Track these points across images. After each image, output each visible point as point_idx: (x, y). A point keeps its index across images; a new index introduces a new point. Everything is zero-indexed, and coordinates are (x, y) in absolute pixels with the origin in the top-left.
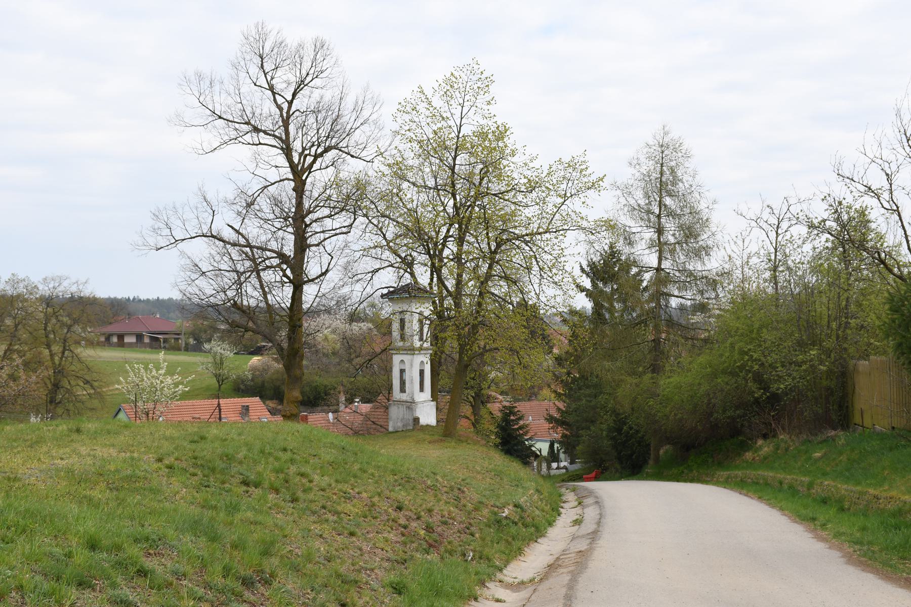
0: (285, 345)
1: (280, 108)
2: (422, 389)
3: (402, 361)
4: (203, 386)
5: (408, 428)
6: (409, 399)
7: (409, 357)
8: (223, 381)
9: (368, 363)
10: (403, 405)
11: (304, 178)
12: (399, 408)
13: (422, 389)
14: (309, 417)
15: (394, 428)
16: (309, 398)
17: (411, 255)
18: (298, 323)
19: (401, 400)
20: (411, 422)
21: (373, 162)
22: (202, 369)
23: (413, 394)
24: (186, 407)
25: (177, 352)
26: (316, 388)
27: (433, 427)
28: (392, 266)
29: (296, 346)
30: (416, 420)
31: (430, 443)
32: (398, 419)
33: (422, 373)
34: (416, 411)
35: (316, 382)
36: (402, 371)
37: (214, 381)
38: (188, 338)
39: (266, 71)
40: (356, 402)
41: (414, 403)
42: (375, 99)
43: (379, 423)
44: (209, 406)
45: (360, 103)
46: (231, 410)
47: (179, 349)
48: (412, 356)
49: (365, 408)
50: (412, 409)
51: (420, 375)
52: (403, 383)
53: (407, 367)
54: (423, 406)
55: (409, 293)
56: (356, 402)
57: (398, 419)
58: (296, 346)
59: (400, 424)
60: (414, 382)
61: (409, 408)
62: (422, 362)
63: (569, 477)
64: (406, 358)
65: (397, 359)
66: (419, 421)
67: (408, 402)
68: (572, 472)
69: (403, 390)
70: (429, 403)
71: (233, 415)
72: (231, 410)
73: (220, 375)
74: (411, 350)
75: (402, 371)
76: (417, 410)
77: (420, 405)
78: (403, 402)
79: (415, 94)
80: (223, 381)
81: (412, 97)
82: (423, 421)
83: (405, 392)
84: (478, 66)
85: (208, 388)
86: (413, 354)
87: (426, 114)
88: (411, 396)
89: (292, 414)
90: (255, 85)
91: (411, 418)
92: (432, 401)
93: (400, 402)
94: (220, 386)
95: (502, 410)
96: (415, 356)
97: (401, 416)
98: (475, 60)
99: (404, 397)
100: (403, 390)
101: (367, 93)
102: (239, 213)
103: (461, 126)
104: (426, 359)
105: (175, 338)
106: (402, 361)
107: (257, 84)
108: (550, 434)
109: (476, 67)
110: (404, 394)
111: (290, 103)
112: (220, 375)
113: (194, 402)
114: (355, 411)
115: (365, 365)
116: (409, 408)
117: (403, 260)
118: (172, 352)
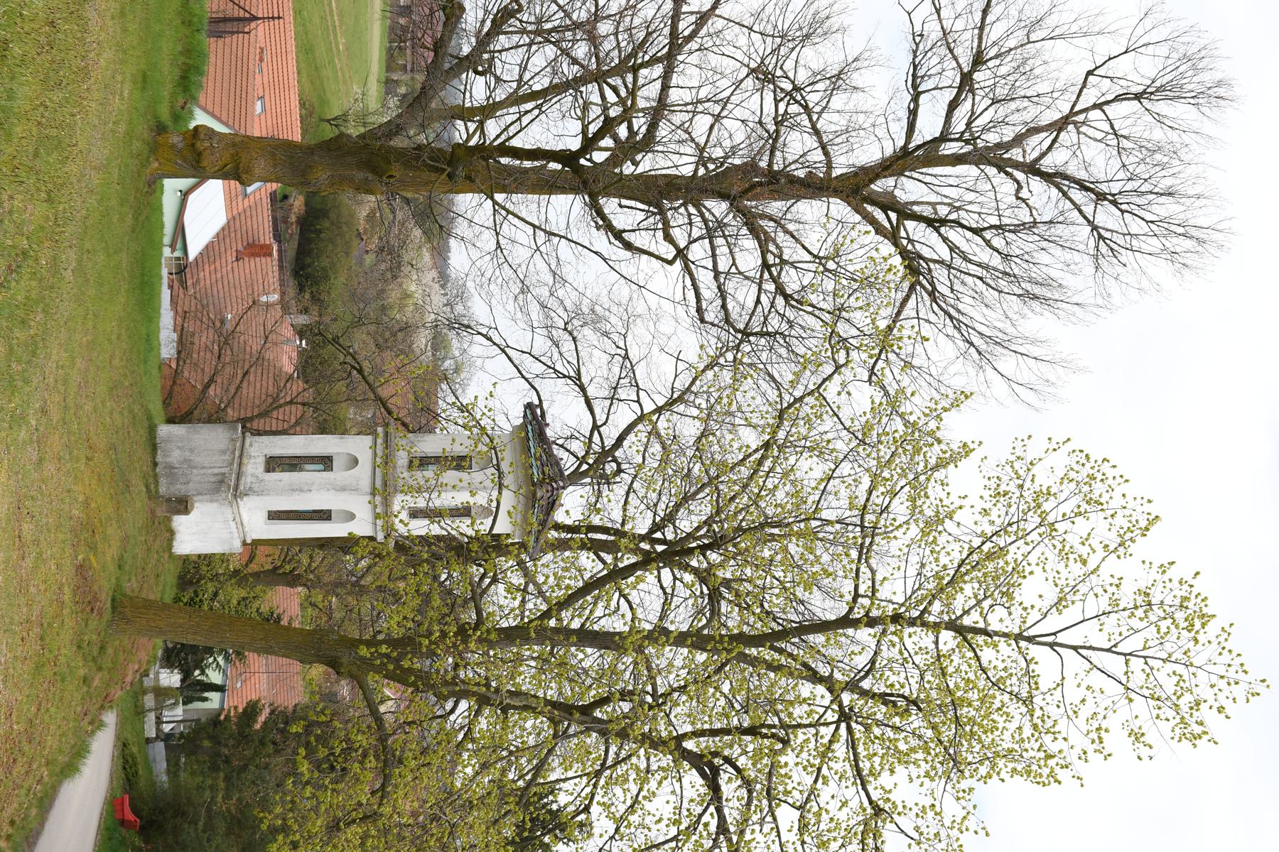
0: (398, 142)
1: (1018, 140)
2: (275, 516)
3: (354, 462)
4: (328, 94)
5: (162, 481)
6: (247, 481)
7: (365, 483)
8: (336, 126)
9: (353, 367)
10: (232, 464)
11: (907, 173)
12: (223, 452)
13: (275, 516)
14: (269, 259)
15: (167, 441)
16: (309, 266)
17: (620, 471)
18: (461, 172)
19: (245, 460)
20: (179, 489)
21: (870, 380)
22: (356, 93)
23: (259, 493)
24: (283, 39)
25: (384, 64)
26: (327, 278)
27: (170, 546)
28: (595, 427)
29: (396, 170)
30: (183, 505)
31: (81, 569)
32: (192, 451)
33: (324, 515)
34: (212, 501)
35: (336, 278)
36: (326, 462)
37: (336, 112)
38: (406, 85)
39: (1105, 108)
40: (301, 341)
41: (235, 496)
42: (1049, 390)
43: (245, 385)
44: (286, 82)
45: (1035, 351)
46: (279, 121)
47: (389, 69)
48: (367, 489)
49: (287, 358)
50: (217, 490)
51: (315, 511)
52: (293, 463)
53: (338, 475)
54: (226, 521)
55: (542, 482)
56: (301, 341)
57: (192, 451)
58: (396, 170)
59: (175, 456)
60: (296, 496)
61: (222, 482)
62: (351, 517)
63: (133, 758)
64: (363, 474)
65: (360, 446)
66: (179, 512)
67: (238, 479)
68: (146, 756)
69: (274, 464)
70: (236, 535)
71: (269, 123)
72: (279, 121)
73: (345, 121)
74: (383, 490)
75: (326, 462)
76: (215, 505)
77: (228, 512)
78: (240, 464)
79: (1140, 509)
80: (336, 126)
81: (1129, 498)
82: (180, 523)
83: (268, 470)
84: (1241, 698)
85: (324, 102)
86: (373, 494)
87: (1068, 537)
88: (256, 487)
89: (200, 154)
90: (1090, 73)
91: (190, 489)
92: (244, 543)
93: (241, 456)
94: (328, 121)
95: (272, 613)
96: (368, 498)
97: (198, 460)
98: (1260, 688)
99: (254, 468)
100: (274, 464)
101: (1060, 370)
102: (757, 16)
103: (1052, 645)
104: (362, 526)
105: (405, 66)
106: (354, 462)
107: (1091, 78)
108: (241, 674)
109: (1240, 691)
110: (261, 468)
111: (1032, 169)
112: (345, 121)
113: (292, 56)
114: (267, 338)
115: (349, 359)
116: (221, 481)
117: (607, 454)
118: (384, 58)
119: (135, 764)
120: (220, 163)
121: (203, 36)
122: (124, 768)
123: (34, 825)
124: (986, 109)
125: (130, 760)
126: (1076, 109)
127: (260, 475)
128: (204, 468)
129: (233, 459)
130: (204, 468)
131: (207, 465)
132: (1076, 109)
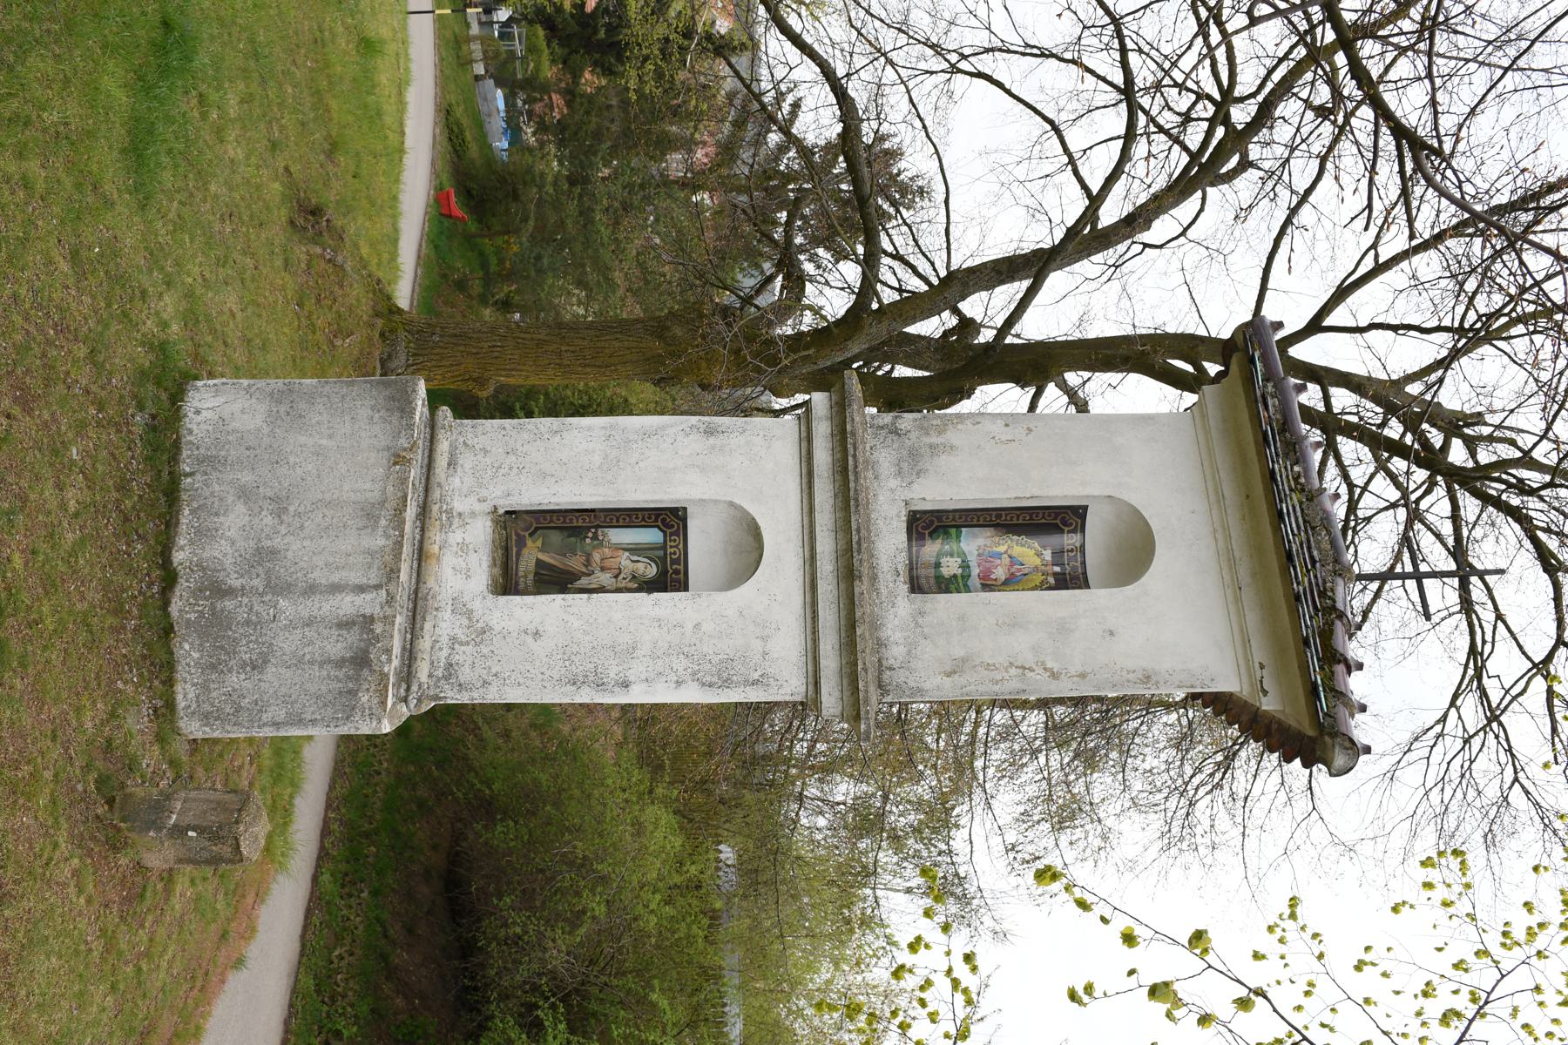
12: (369, 515)
19: (435, 537)
32: (280, 507)
61: (361, 661)
63: (459, 124)
78: (421, 554)
119: (462, 132)
120: (1075, 105)
121: (1169, 1006)
122: (450, 139)
123: (164, 657)
124: (796, 40)
125: (456, 130)
126: (1331, 462)
127: (477, 605)
128: (311, 590)
129: (399, 544)
130: (311, 590)
131: (320, 577)
132: (1331, 462)
